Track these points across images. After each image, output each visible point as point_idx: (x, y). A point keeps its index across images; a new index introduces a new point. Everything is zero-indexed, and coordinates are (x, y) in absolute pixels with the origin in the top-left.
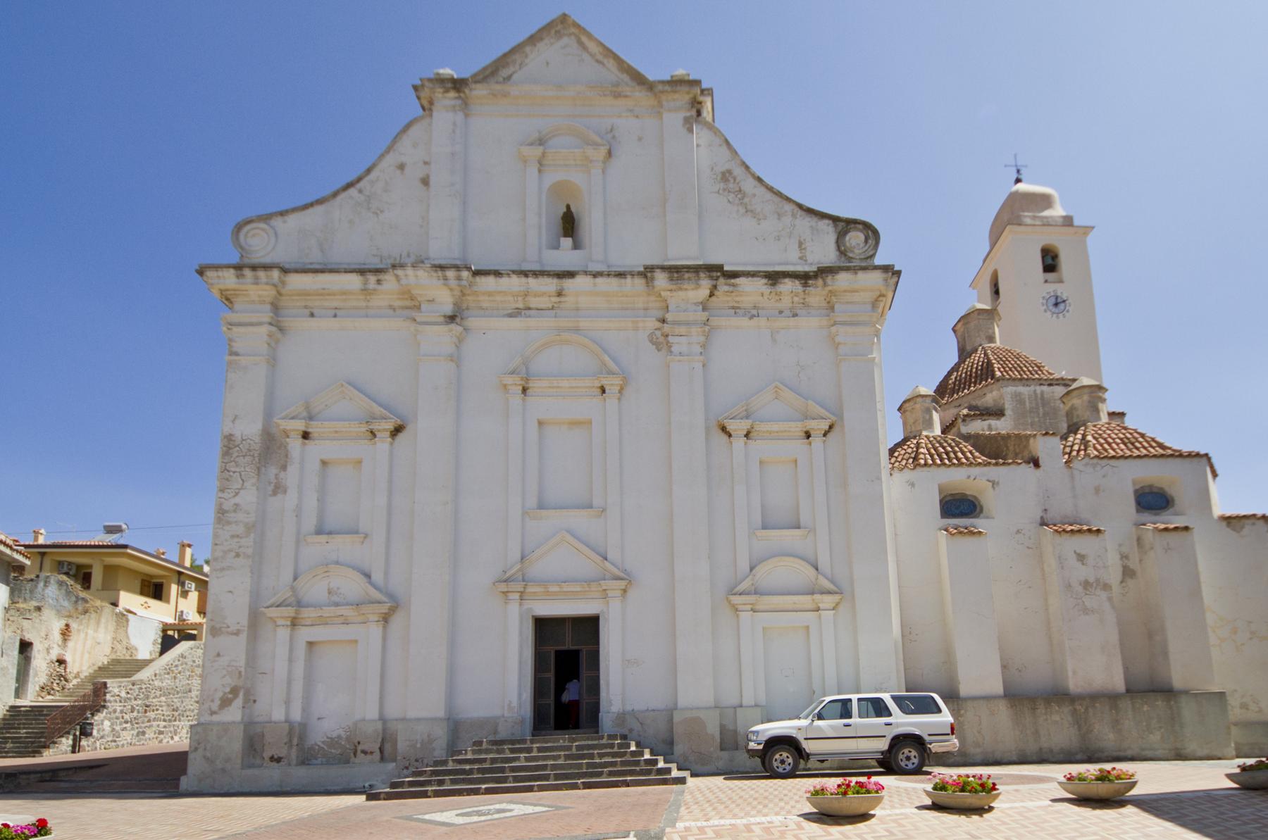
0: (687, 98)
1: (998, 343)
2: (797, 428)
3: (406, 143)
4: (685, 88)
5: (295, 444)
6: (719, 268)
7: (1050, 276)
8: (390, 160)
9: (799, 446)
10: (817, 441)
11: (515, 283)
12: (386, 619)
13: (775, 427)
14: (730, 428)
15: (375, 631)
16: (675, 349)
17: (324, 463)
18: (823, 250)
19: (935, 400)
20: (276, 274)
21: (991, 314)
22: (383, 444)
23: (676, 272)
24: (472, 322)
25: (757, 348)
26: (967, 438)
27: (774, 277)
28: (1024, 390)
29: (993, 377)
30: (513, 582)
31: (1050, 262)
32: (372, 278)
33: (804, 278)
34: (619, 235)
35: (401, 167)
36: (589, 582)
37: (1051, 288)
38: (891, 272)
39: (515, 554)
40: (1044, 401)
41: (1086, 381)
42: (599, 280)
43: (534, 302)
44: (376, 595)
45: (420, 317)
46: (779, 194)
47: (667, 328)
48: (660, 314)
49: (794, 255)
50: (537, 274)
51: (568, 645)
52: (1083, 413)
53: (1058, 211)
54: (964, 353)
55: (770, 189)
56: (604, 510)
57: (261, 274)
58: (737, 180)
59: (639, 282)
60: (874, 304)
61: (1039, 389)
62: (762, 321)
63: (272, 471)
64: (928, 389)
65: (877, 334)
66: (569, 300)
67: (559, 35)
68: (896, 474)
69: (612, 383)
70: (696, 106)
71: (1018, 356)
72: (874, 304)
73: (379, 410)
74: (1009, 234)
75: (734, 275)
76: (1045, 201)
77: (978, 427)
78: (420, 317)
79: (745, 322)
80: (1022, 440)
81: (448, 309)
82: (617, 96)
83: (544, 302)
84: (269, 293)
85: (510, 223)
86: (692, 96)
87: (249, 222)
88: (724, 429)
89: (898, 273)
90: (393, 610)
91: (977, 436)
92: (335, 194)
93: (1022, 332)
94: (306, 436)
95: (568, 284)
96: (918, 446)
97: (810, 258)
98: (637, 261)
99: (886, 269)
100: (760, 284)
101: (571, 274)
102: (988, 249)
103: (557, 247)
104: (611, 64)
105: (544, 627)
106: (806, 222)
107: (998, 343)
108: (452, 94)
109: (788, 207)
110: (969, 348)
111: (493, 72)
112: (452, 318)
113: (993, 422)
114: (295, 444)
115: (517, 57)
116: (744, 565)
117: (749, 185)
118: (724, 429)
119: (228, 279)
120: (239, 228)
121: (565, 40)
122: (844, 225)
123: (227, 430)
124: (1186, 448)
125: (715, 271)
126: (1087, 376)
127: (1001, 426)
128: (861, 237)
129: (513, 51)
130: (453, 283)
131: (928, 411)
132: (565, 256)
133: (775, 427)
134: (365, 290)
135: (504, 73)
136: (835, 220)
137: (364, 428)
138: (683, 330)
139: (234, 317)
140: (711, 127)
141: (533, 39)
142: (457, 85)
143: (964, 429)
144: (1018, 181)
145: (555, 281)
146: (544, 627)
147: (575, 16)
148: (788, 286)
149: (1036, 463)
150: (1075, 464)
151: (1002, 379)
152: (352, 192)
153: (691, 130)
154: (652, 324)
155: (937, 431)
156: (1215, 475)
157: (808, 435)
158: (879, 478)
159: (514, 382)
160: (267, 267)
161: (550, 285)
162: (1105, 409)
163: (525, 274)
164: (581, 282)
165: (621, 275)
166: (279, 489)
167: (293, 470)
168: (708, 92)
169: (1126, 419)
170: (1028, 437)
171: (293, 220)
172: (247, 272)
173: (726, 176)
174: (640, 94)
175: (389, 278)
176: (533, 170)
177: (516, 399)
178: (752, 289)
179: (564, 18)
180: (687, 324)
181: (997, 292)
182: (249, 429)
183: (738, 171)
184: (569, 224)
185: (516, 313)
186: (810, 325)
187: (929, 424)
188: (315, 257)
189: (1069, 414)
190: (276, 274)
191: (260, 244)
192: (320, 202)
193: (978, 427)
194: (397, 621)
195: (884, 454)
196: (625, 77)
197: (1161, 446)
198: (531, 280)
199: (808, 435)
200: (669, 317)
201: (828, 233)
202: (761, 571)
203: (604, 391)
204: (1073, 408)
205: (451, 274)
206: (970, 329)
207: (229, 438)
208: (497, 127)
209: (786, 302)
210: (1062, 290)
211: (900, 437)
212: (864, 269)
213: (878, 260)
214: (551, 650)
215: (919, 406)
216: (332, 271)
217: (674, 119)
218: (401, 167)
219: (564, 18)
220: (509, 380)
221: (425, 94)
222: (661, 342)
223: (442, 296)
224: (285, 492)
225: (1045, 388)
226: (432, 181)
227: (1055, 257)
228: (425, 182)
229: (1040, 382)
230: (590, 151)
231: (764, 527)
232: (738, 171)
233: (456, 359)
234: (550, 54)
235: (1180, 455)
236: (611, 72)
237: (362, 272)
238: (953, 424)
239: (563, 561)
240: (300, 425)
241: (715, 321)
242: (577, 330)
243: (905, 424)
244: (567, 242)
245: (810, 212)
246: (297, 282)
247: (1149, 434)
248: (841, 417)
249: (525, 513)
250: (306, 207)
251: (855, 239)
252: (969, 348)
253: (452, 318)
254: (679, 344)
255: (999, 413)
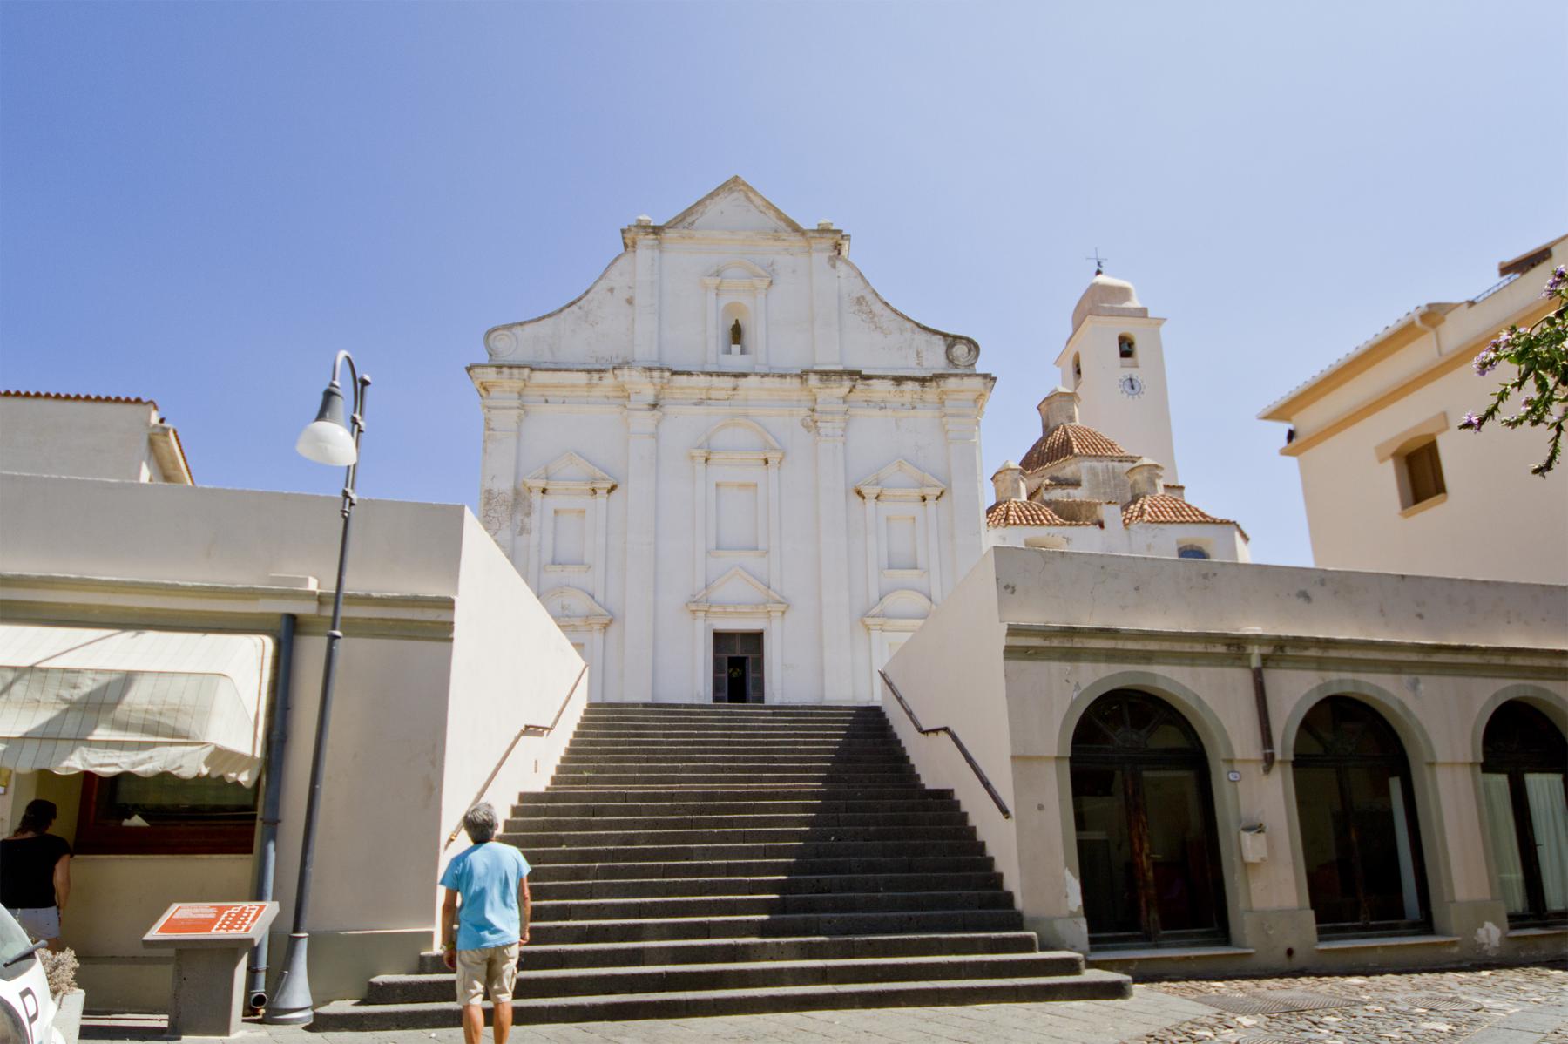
0: (831, 242)
1: (1078, 422)
2: (917, 493)
3: (614, 271)
4: (830, 235)
5: (537, 497)
6: (858, 373)
7: (1127, 360)
8: (604, 284)
9: (919, 506)
10: (931, 503)
11: (702, 381)
12: (606, 627)
13: (898, 492)
14: (864, 492)
15: (598, 636)
16: (822, 432)
17: (556, 512)
18: (935, 359)
19: (1022, 473)
20: (526, 371)
21: (1071, 397)
22: (602, 498)
23: (825, 375)
24: (670, 409)
25: (884, 432)
26: (1048, 504)
27: (899, 380)
28: (1099, 466)
29: (1072, 452)
30: (697, 605)
31: (1127, 348)
32: (596, 376)
33: (923, 381)
34: (778, 341)
35: (611, 290)
36: (757, 606)
37: (1128, 372)
38: (989, 378)
39: (700, 584)
40: (1115, 475)
41: (1146, 461)
42: (766, 379)
43: (714, 394)
44: (599, 610)
45: (630, 405)
46: (901, 315)
47: (816, 416)
48: (811, 405)
49: (912, 362)
50: (719, 374)
51: (738, 654)
52: (1143, 487)
53: (1135, 303)
54: (1048, 430)
55: (895, 312)
56: (767, 552)
57: (516, 371)
58: (868, 304)
59: (796, 381)
60: (976, 401)
61: (1110, 464)
62: (889, 412)
63: (519, 517)
64: (1015, 464)
65: (978, 423)
66: (741, 393)
67: (731, 191)
68: (992, 530)
69: (774, 457)
70: (837, 247)
71: (1094, 435)
72: (976, 401)
73: (599, 474)
74: (1089, 323)
75: (869, 378)
76: (1124, 293)
77: (1058, 494)
78: (630, 405)
79: (876, 412)
80: (1091, 506)
81: (651, 400)
82: (777, 239)
83: (723, 395)
84: (519, 385)
85: (698, 338)
86: (835, 240)
87: (495, 330)
88: (859, 493)
89: (994, 379)
90: (611, 621)
91: (1057, 503)
92: (561, 310)
93: (1100, 412)
94: (544, 491)
95: (742, 382)
96: (1008, 509)
97: (925, 364)
98: (796, 363)
99: (985, 376)
100: (889, 384)
101: (745, 375)
102: (1070, 332)
103: (729, 352)
104: (771, 213)
105: (721, 639)
106: (923, 337)
107: (1078, 422)
108: (652, 236)
109: (909, 325)
110: (1052, 425)
111: (683, 220)
112: (654, 406)
113: (1071, 491)
114: (537, 497)
115: (700, 208)
116: (875, 596)
117: (878, 308)
118: (859, 493)
119: (490, 375)
120: (489, 333)
121: (735, 195)
122: (952, 340)
123: (487, 486)
124: (1220, 517)
125: (856, 375)
126: (137, 829)
127: (1078, 495)
128: (965, 349)
129: (698, 204)
130: (657, 380)
131: (1016, 481)
132: (736, 360)
133: (898, 492)
134: (590, 385)
135: (690, 219)
136: (945, 336)
137: (589, 487)
138: (829, 418)
139: (491, 403)
140: (847, 263)
141: (712, 195)
142: (656, 230)
143: (1047, 497)
144: (1098, 272)
145: (733, 379)
146: (721, 639)
147: (744, 178)
148: (909, 386)
149: (1102, 526)
150: (1133, 526)
151: (1081, 455)
152: (574, 308)
153: (834, 266)
154: (804, 412)
155: (1024, 498)
156: (1246, 538)
157: (924, 499)
158: (979, 532)
159: (700, 454)
160: (520, 367)
161: (728, 382)
162: (1160, 483)
163: (710, 374)
164: (752, 380)
165: (782, 376)
166: (523, 530)
167: (535, 516)
168: (848, 237)
169: (1185, 492)
170: (1096, 505)
171: (528, 328)
172: (505, 370)
173: (860, 301)
174: (795, 239)
175: (608, 376)
176: (712, 295)
177: (700, 466)
178: (882, 388)
179: (736, 179)
180: (832, 413)
181: (1079, 372)
182: (504, 485)
183: (870, 297)
184: (737, 334)
185: (700, 403)
186: (926, 416)
187: (1017, 492)
188: (546, 358)
189: (1133, 487)
190: (526, 371)
191: (508, 348)
192: (549, 316)
193: (1058, 494)
194: (613, 629)
195: (983, 513)
196: (783, 224)
197: (1202, 514)
198: (715, 380)
199: (924, 499)
200: (818, 408)
201: (940, 345)
202: (887, 601)
203: (767, 462)
204: (1135, 482)
205: (656, 374)
206: (1053, 407)
207: (489, 492)
208: (683, 260)
209: (907, 398)
210: (1135, 373)
211: (993, 502)
212: (969, 376)
213: (980, 368)
214: (725, 656)
215: (1009, 476)
216: (567, 370)
217: (821, 257)
218: (611, 290)
219: (736, 179)
220: (696, 453)
221: (629, 236)
222: (812, 425)
223: (645, 388)
224: (529, 533)
225: (1116, 464)
226: (637, 301)
227: (1131, 344)
228: (630, 302)
229: (1112, 458)
230: (756, 281)
231: (890, 567)
232: (870, 297)
233: (655, 436)
234: (725, 203)
235: (1214, 522)
236: (772, 220)
237: (589, 371)
238: (1037, 491)
239: (734, 590)
240: (542, 484)
241: (852, 411)
242: (746, 416)
243: (997, 491)
244: (736, 348)
245: (925, 329)
246: (539, 377)
247: (1194, 505)
248: (950, 486)
249: (708, 552)
250: (539, 319)
251: (960, 350)
252: (1052, 425)
253: (654, 406)
254: (826, 428)
255: (1076, 484)
